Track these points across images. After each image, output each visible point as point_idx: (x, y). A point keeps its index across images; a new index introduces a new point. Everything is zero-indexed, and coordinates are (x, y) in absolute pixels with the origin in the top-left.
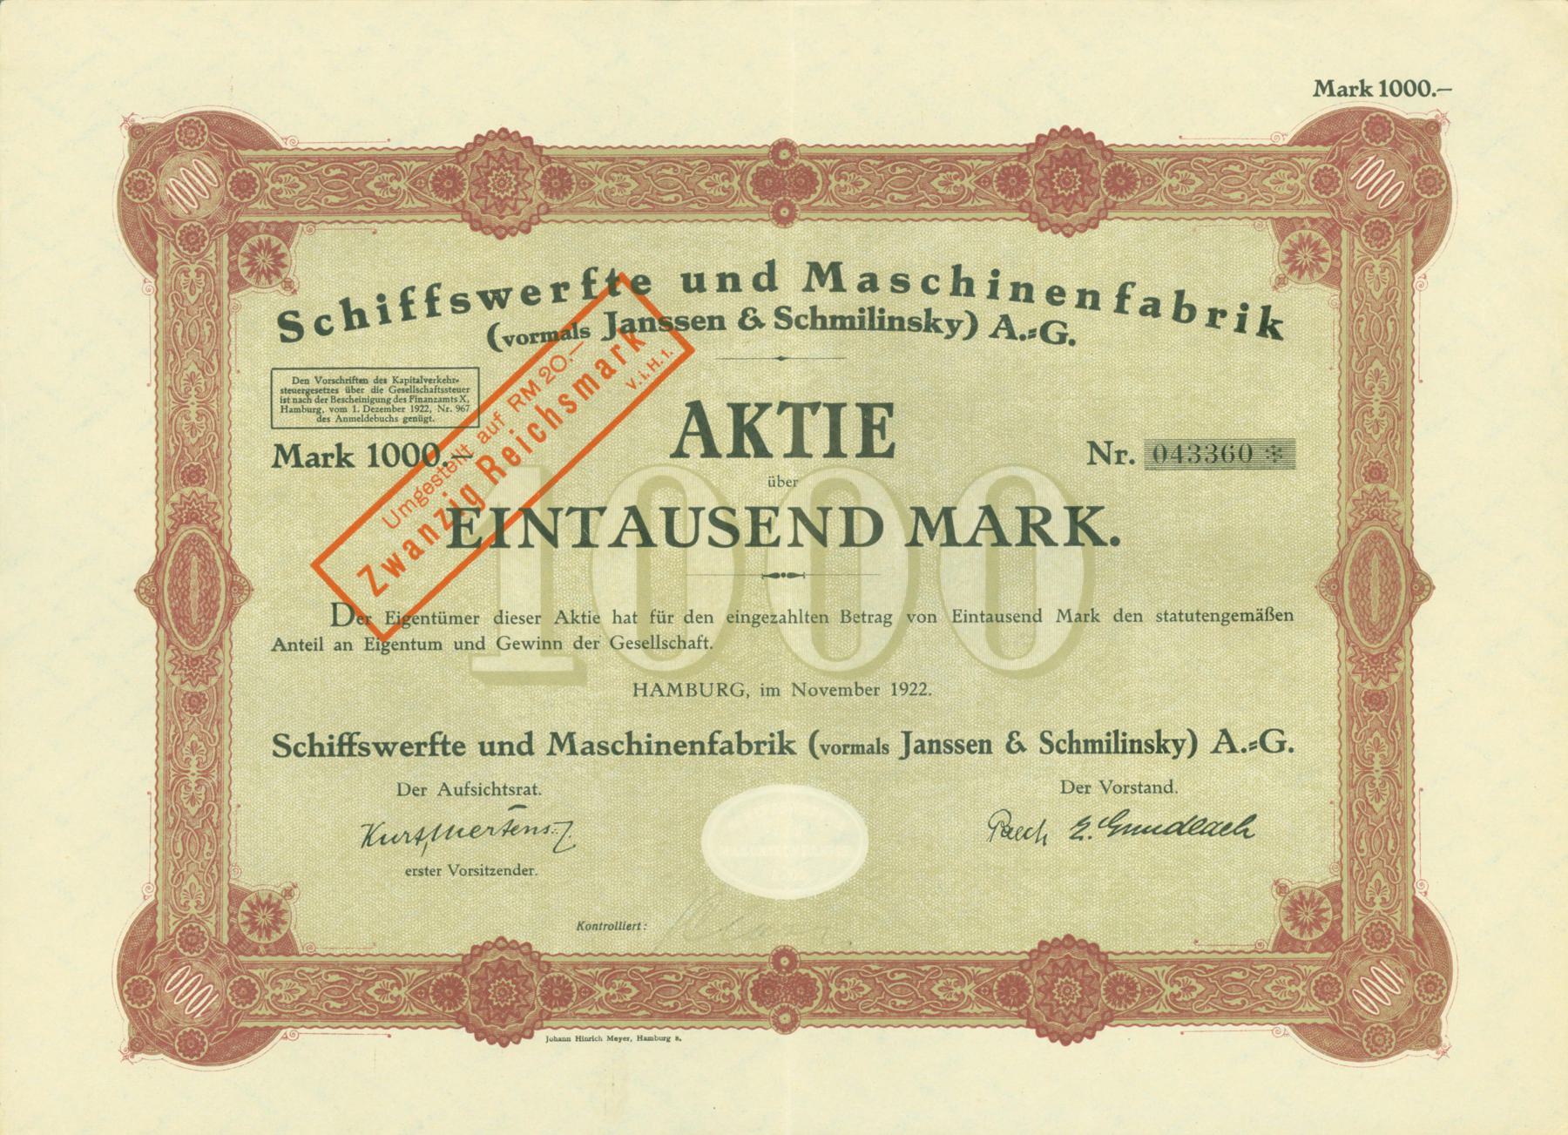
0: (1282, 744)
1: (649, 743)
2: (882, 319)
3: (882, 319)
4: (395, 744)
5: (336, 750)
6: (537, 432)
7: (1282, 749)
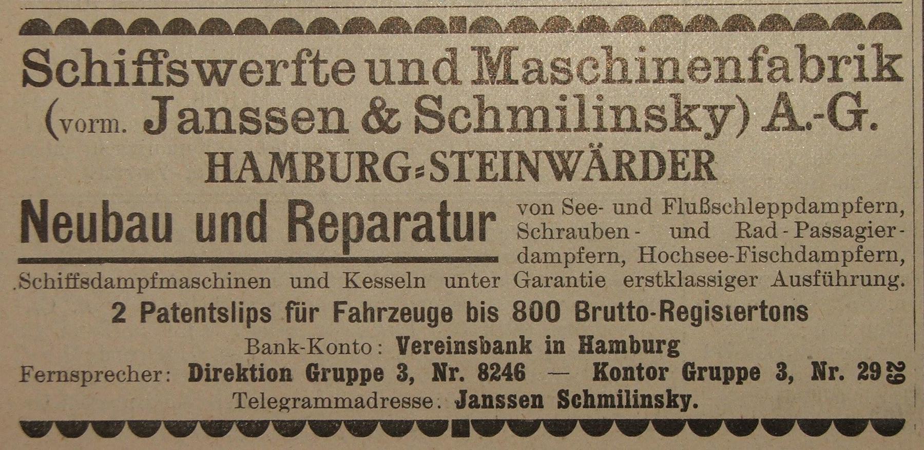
0: (858, 115)
1: (449, 343)
2: (635, 397)
3: (635, 397)
4: (230, 63)
5: (64, 284)
6: (577, 402)
7: (858, 123)
